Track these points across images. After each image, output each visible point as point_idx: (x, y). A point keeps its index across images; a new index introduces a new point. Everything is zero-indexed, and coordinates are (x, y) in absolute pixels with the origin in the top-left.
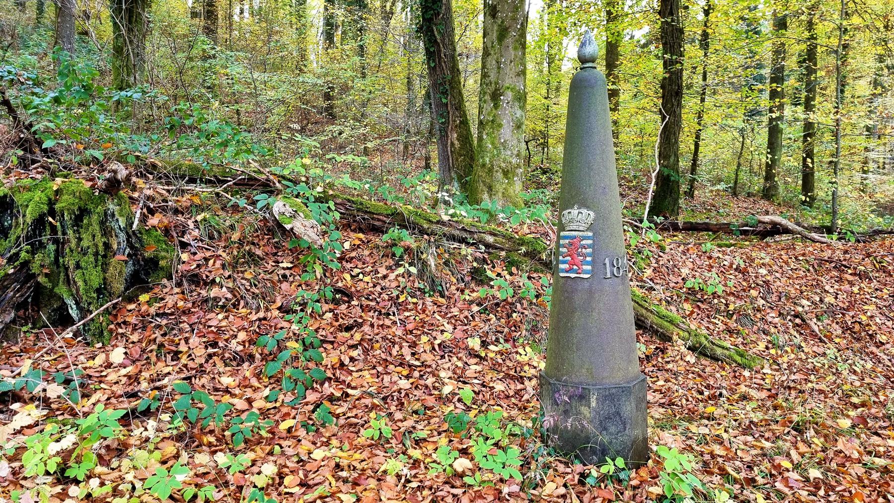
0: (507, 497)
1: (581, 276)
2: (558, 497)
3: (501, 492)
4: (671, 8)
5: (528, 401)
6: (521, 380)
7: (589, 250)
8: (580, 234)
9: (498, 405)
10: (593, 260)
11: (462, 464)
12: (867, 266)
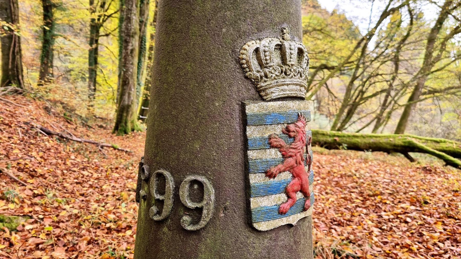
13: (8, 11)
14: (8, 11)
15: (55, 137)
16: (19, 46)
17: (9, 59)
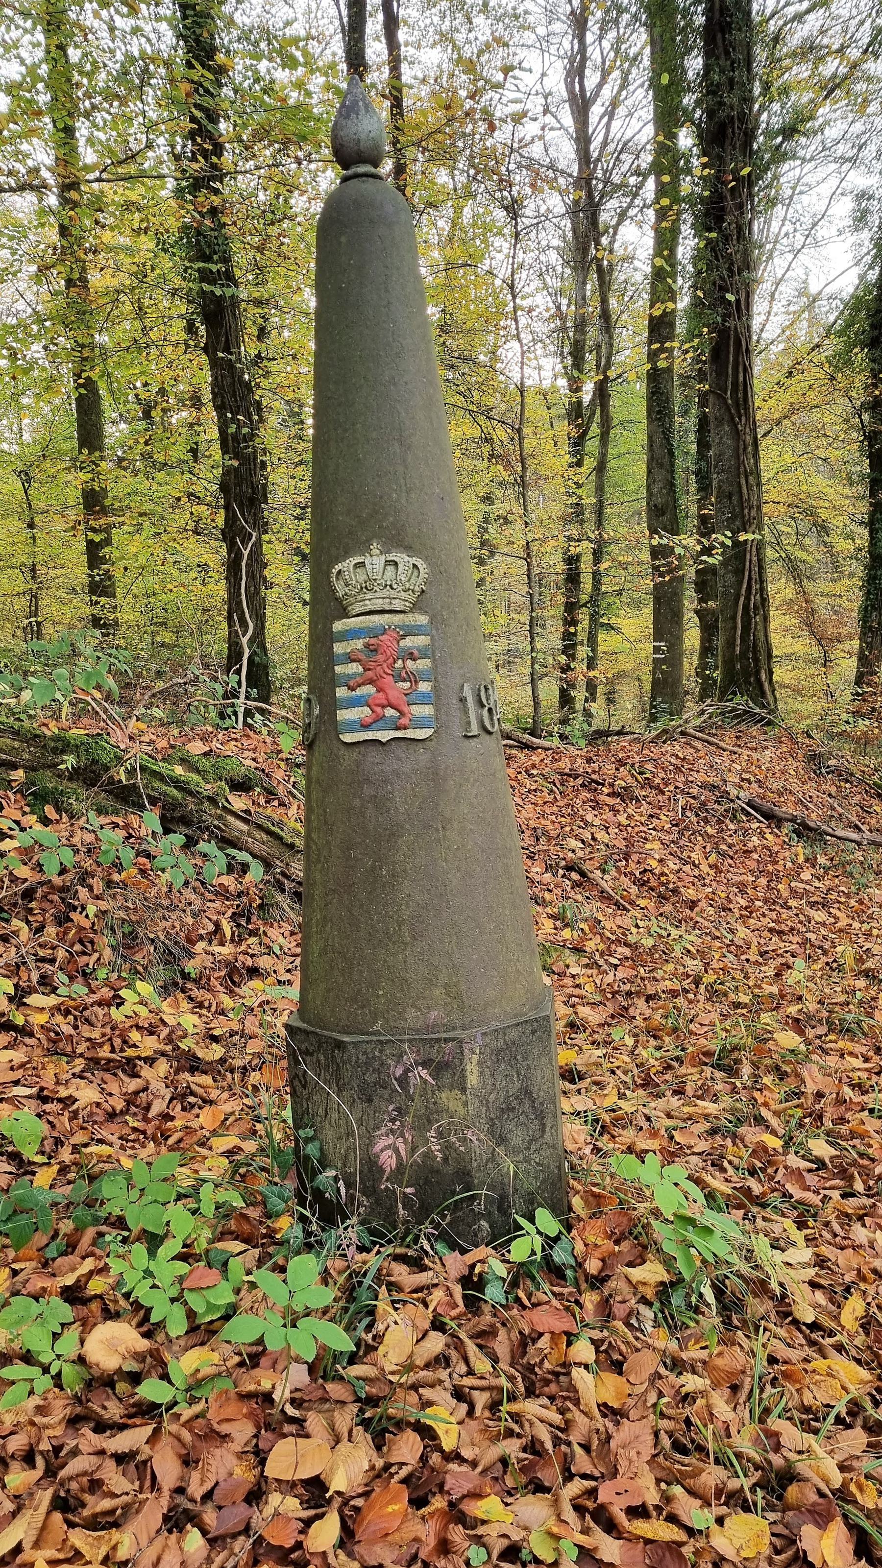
0: (290, 1411)
1: (410, 734)
2: (427, 1366)
3: (267, 1398)
4: (227, 340)
5: (167, 1117)
6: (130, 1068)
7: (423, 664)
8: (396, 619)
9: (101, 1141)
10: (436, 689)
11: (112, 1344)
12: (624, 779)
13: (735, 498)
14: (735, 498)
15: (787, 827)
16: (762, 590)
17: (735, 628)
